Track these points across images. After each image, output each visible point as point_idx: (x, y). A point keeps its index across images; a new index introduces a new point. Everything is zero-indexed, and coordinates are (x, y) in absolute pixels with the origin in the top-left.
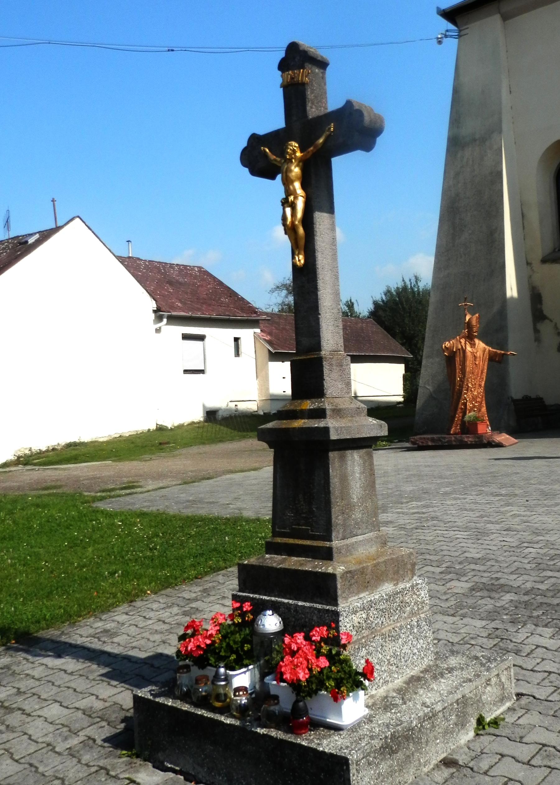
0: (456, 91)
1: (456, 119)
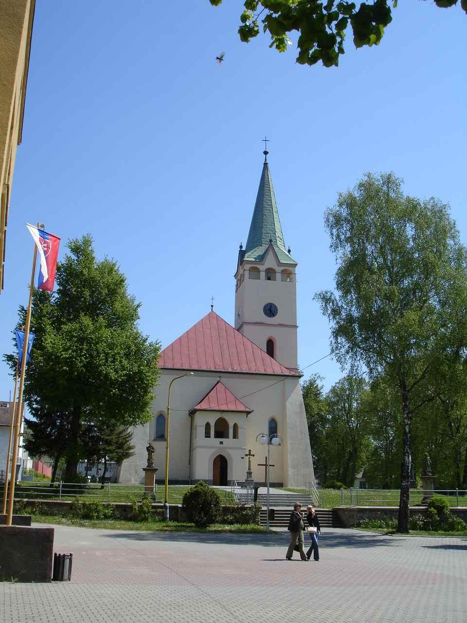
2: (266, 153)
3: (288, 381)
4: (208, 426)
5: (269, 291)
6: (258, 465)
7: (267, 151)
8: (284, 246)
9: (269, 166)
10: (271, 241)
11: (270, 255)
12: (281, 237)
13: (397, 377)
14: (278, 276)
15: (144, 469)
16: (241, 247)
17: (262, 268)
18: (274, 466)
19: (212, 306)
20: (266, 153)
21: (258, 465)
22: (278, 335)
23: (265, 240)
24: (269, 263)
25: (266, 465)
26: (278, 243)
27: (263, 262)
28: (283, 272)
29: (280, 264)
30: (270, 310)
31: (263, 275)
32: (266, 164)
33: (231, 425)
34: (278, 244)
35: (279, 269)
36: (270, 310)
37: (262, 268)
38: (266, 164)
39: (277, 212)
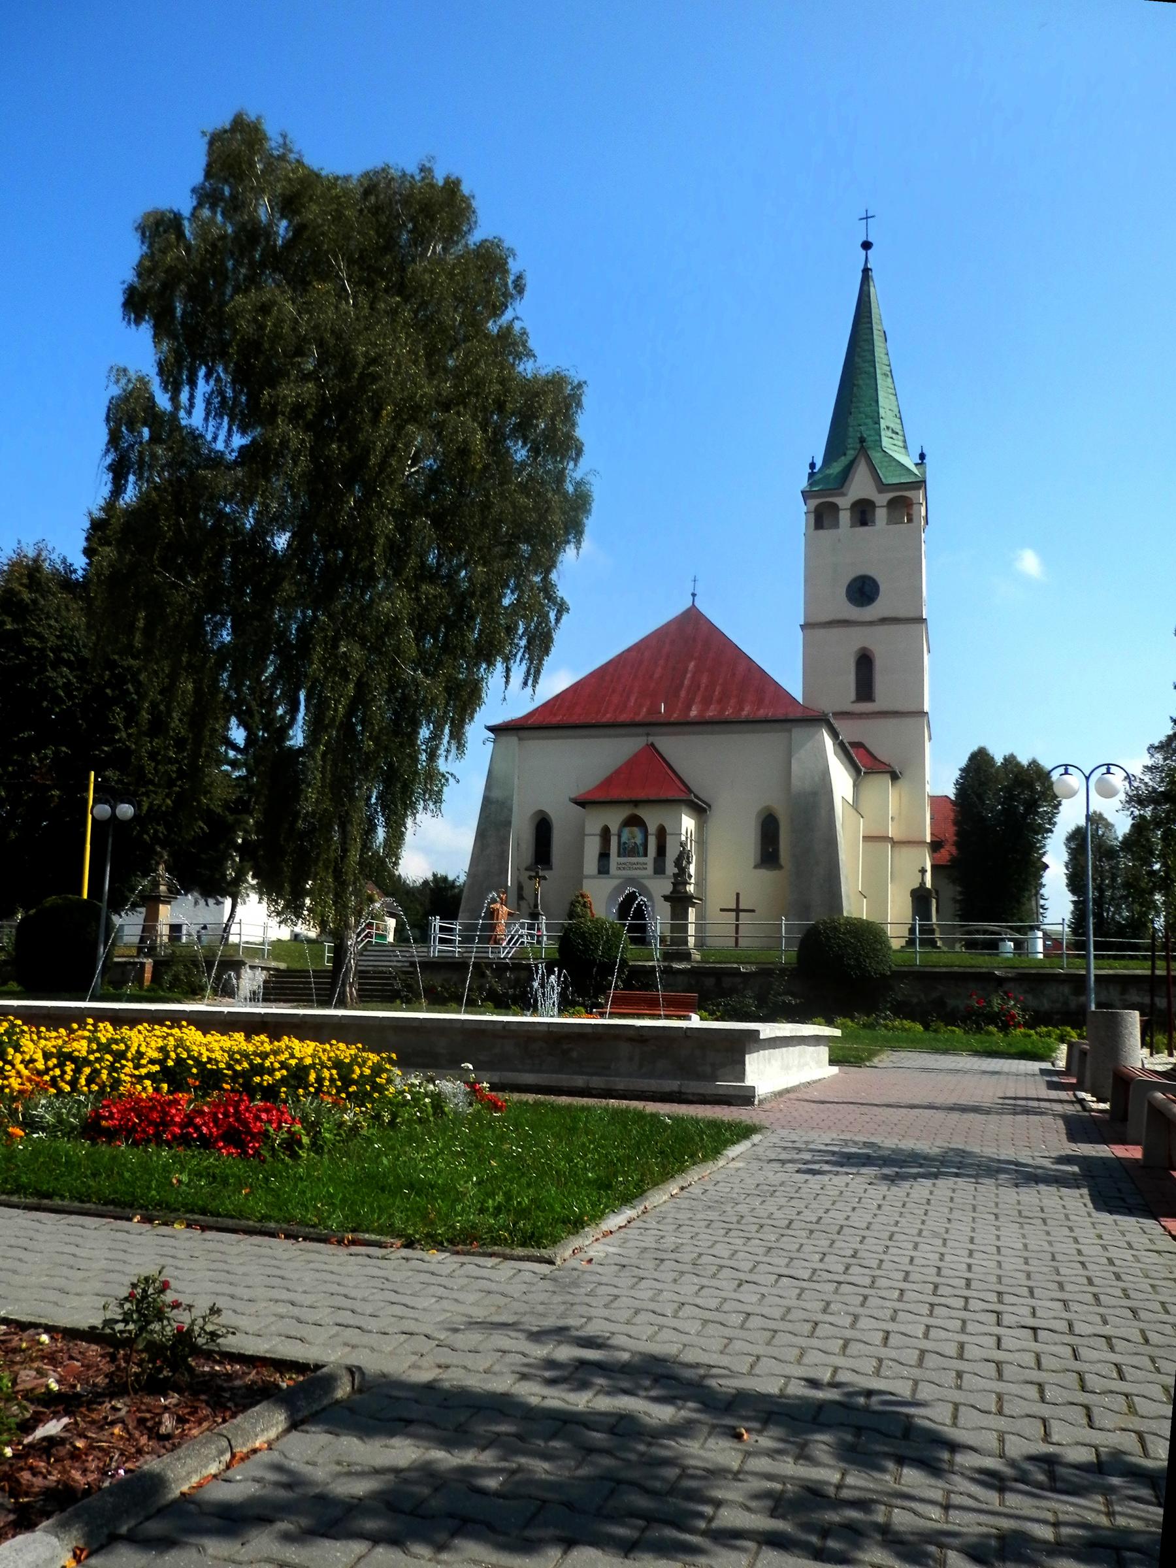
0: (490, 772)
1: (488, 787)
2: (867, 245)
3: (798, 733)
4: (605, 833)
5: (866, 549)
6: (722, 910)
7: (870, 240)
8: (905, 447)
9: (874, 274)
10: (862, 440)
11: (862, 470)
12: (898, 428)
13: (224, 768)
14: (881, 514)
15: (666, 898)
16: (812, 466)
17: (844, 502)
18: (753, 911)
19: (694, 595)
20: (867, 245)
21: (722, 910)
22: (879, 641)
23: (852, 442)
24: (860, 486)
25: (737, 910)
26: (886, 442)
27: (844, 490)
28: (893, 504)
29: (882, 487)
30: (863, 590)
31: (845, 517)
32: (866, 271)
33: (652, 828)
34: (884, 444)
35: (882, 499)
36: (863, 590)
37: (844, 502)
38: (866, 271)
39: (890, 374)
